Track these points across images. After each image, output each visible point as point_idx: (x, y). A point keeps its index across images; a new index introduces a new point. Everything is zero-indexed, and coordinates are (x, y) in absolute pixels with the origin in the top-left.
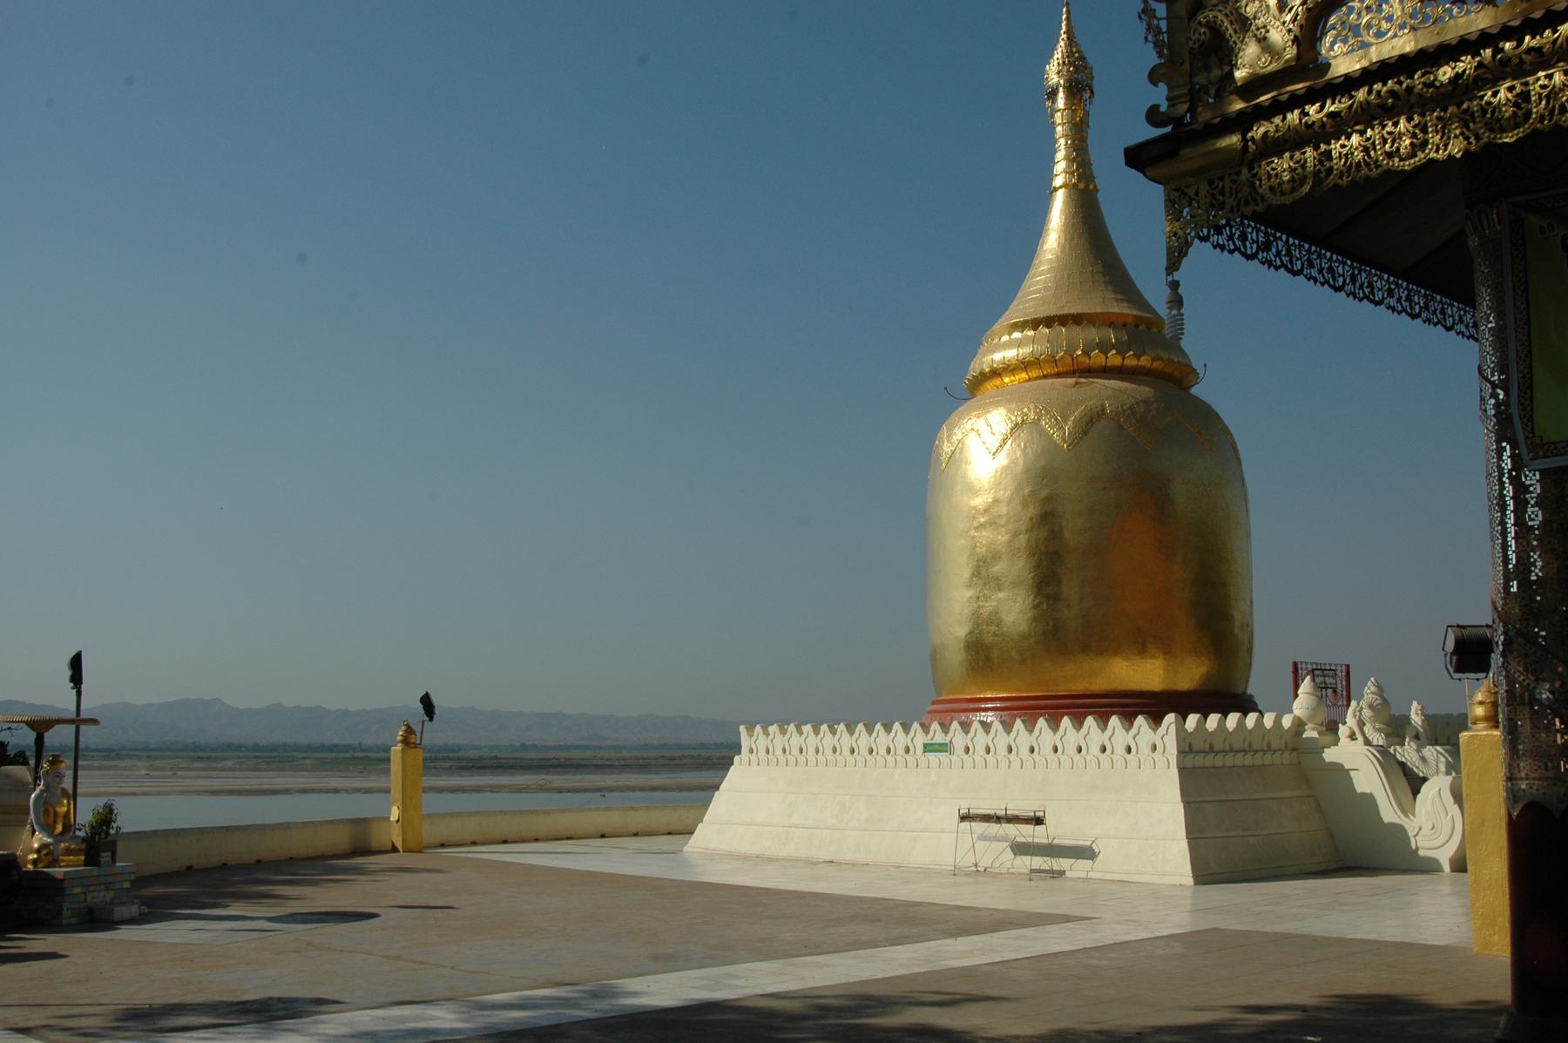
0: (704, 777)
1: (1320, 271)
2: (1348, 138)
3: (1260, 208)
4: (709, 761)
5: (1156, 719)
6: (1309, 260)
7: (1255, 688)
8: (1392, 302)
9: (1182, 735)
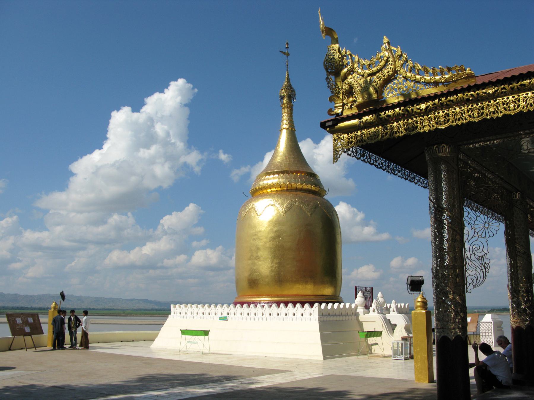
0: (157, 320)
1: (379, 164)
2: (393, 123)
3: (364, 143)
4: (163, 312)
5: (312, 304)
7: (343, 294)
8: (400, 174)
9: (320, 310)
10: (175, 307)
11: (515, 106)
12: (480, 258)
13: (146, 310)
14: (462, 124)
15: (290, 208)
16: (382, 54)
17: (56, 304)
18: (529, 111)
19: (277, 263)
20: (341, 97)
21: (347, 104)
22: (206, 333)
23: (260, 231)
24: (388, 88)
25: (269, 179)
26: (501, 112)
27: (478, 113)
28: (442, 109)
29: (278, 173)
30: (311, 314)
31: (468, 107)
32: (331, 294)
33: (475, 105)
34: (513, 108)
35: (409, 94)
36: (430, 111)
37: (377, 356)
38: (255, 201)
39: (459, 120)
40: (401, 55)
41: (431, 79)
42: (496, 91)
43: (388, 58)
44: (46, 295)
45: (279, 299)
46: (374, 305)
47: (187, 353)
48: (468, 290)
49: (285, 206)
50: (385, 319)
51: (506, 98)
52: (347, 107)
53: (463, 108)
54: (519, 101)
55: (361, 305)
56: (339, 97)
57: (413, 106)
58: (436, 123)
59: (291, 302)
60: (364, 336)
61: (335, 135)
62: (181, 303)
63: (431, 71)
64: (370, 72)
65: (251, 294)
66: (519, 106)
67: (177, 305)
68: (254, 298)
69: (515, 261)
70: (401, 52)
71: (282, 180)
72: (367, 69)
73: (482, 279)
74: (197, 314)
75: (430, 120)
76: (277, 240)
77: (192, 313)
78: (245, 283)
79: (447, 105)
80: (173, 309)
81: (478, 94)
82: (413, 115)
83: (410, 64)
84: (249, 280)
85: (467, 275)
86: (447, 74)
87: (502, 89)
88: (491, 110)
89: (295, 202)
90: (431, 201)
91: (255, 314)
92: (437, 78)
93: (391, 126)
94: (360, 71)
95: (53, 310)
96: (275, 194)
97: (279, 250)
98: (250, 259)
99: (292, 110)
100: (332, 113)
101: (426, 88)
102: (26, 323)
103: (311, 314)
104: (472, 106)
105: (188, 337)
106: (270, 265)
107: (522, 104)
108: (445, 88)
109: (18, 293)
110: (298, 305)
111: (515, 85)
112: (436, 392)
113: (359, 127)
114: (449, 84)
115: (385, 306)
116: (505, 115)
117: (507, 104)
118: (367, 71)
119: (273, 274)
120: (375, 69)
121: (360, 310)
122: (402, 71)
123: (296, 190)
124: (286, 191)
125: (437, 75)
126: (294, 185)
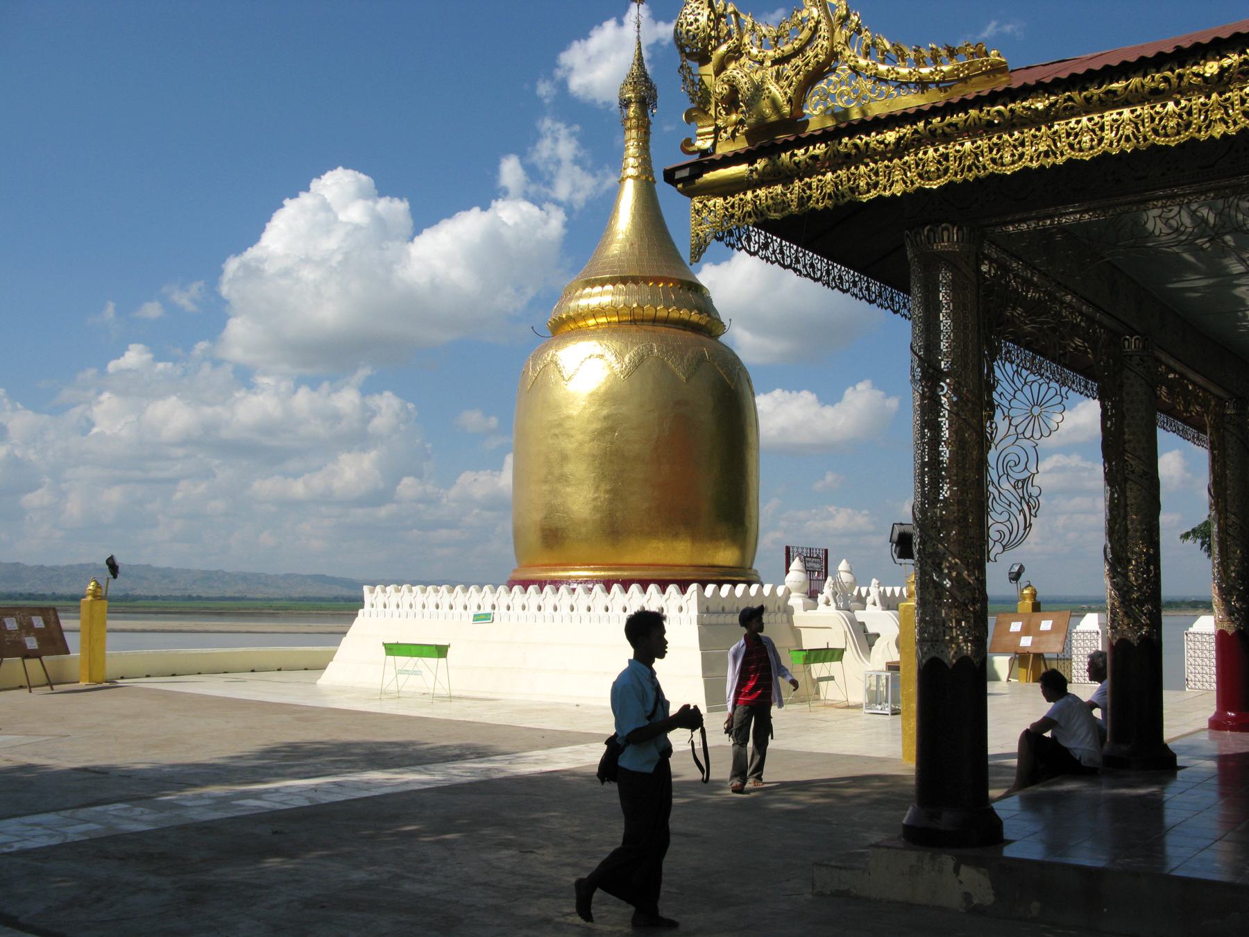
1: (804, 266)
2: (824, 174)
4: (343, 607)
5: (683, 586)
6: (797, 258)
8: (856, 290)
9: (701, 600)
10: (372, 592)
11: (1092, 140)
12: (1020, 484)
13: (321, 599)
14: (977, 178)
15: (638, 364)
16: (805, 13)
17: (98, 586)
18: (1123, 152)
19: (607, 492)
20: (712, 112)
21: (725, 128)
22: (441, 651)
23: (568, 417)
24: (816, 93)
25: (590, 296)
26: (1062, 154)
27: (1013, 155)
28: (933, 145)
29: (613, 281)
30: (681, 609)
31: (990, 139)
32: (731, 564)
33: (1006, 137)
34: (1088, 145)
35: (846, 112)
36: (907, 148)
37: (831, 705)
38: (558, 347)
39: (970, 169)
40: (847, 17)
41: (910, 73)
42: (1052, 105)
43: (818, 22)
44: (89, 565)
45: (611, 573)
46: (827, 590)
47: (398, 696)
48: (992, 557)
49: (627, 359)
50: (853, 621)
51: (1073, 120)
52: (724, 136)
53: (979, 142)
54: (1102, 129)
55: (798, 590)
56: (706, 113)
57: (868, 135)
58: (920, 176)
59: (617, 581)
60: (802, 661)
61: (696, 200)
62: (387, 584)
63: (912, 55)
64: (778, 54)
65: (546, 561)
66: (1101, 140)
67: (378, 588)
68: (555, 570)
69: (1123, 493)
70: (848, 10)
71: (622, 298)
72: (771, 47)
73: (1021, 531)
74: (424, 606)
75: (906, 167)
76: (608, 438)
77: (411, 606)
78: (534, 538)
79: (944, 134)
80: (368, 597)
81: (1012, 111)
82: (868, 157)
83: (867, 37)
84: (543, 530)
85: (990, 522)
86: (947, 64)
87: (1065, 101)
88: (1041, 149)
89: (652, 350)
90: (915, 353)
91: (555, 609)
92: (925, 71)
93: (820, 181)
94: (754, 51)
95: (90, 598)
96: (604, 331)
97: (613, 460)
98: (546, 482)
99: (647, 133)
100: (692, 149)
101: (899, 94)
102: (28, 628)
103: (681, 609)
104: (1000, 138)
105: (401, 660)
106: (591, 495)
107: (1109, 135)
108: (942, 95)
109: (21, 561)
110: (672, 588)
111: (1095, 92)
112: (913, 782)
113: (749, 181)
114: (950, 87)
115: (855, 593)
116: (1070, 160)
117: (1076, 135)
118: (770, 53)
119: (598, 516)
120: (788, 48)
121: (796, 601)
122: (847, 53)
123: (655, 321)
124: (631, 323)
125: (926, 65)
126: (649, 310)
